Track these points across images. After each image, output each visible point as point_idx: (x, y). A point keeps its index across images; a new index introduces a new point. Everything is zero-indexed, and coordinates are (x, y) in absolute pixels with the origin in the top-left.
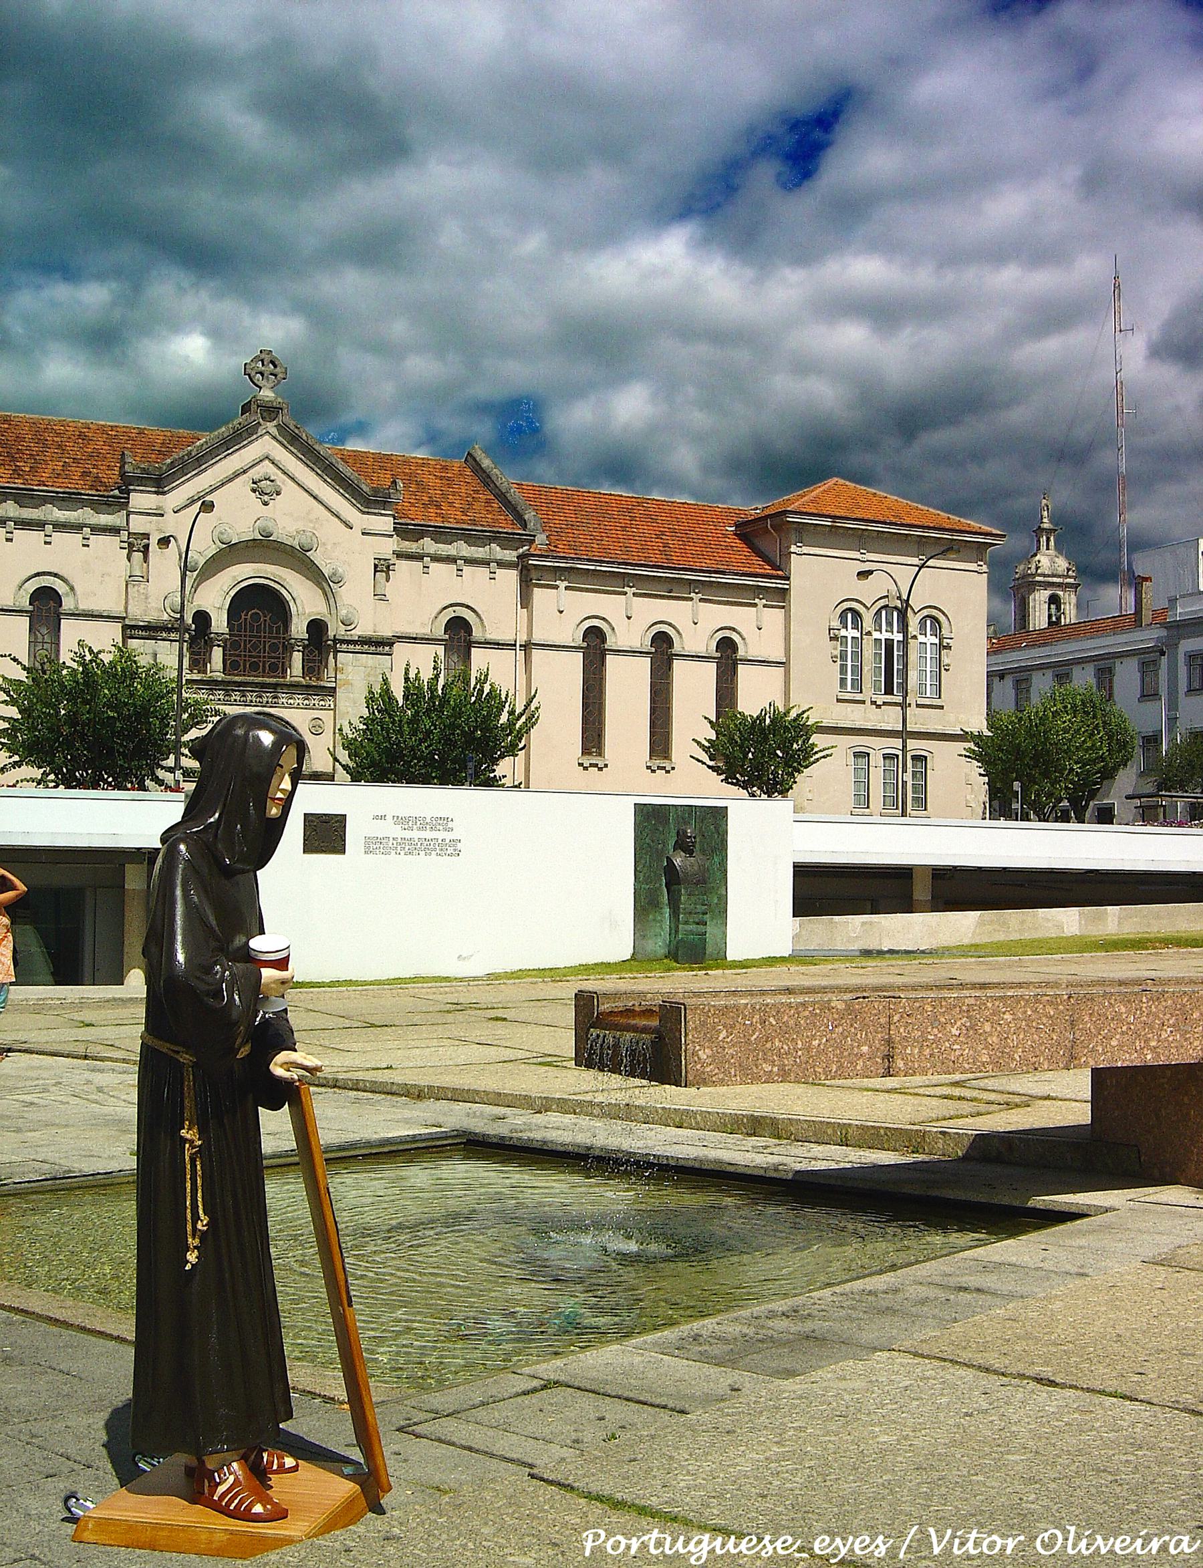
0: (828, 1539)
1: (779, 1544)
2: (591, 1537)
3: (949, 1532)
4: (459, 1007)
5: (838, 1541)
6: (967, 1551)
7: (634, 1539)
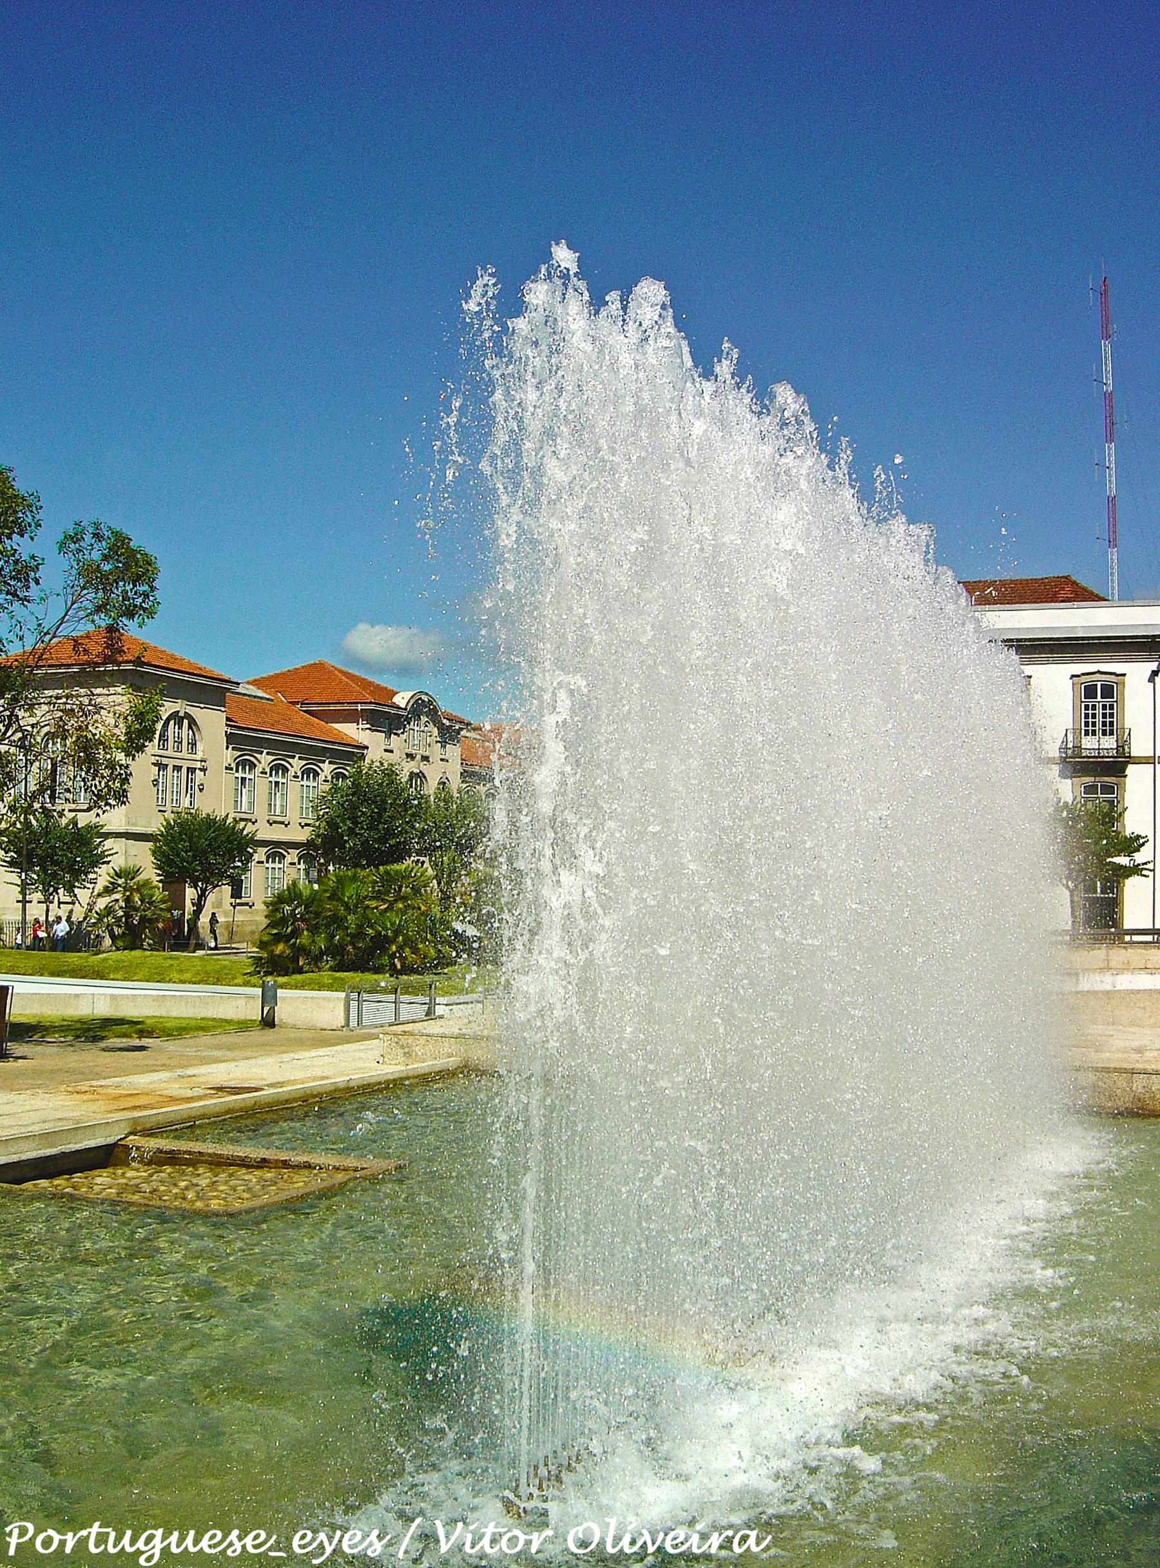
0: (310, 1535)
1: (249, 1541)
2: (16, 1532)
6: (621, 1550)
7: (70, 1534)
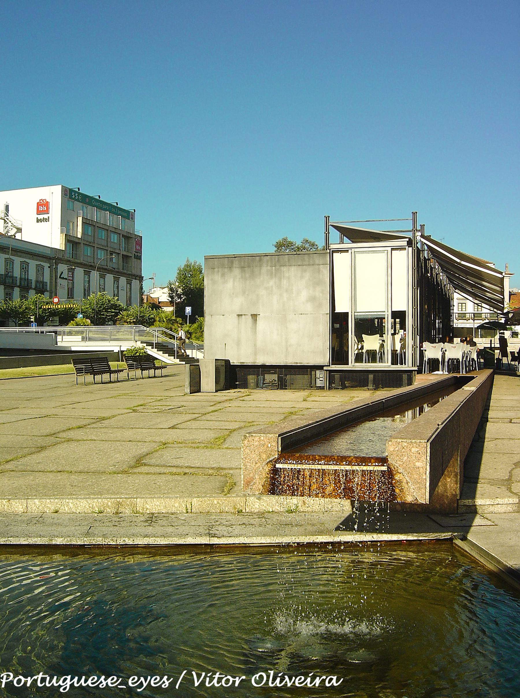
2: (5, 677)
3: (204, 674)
4: (241, 399)
5: (142, 679)
